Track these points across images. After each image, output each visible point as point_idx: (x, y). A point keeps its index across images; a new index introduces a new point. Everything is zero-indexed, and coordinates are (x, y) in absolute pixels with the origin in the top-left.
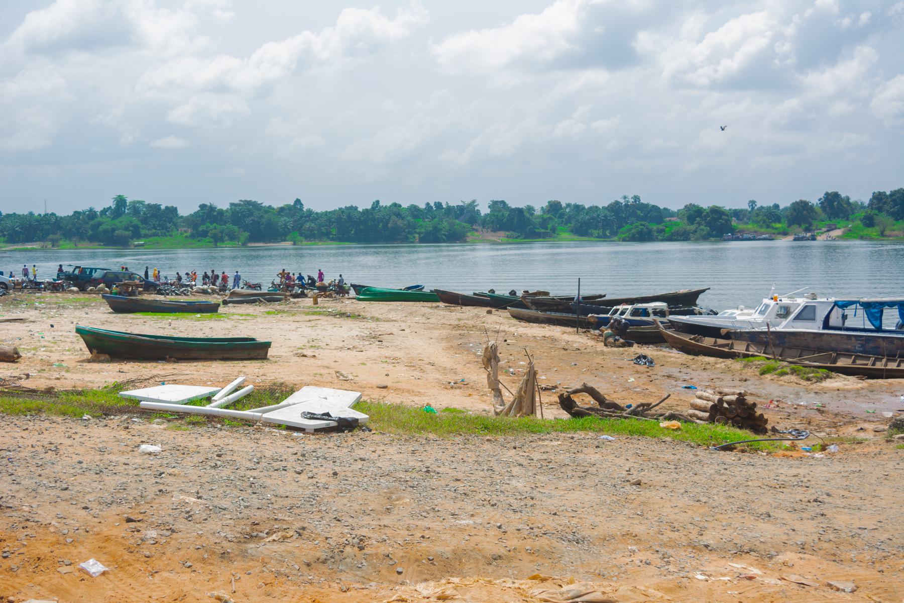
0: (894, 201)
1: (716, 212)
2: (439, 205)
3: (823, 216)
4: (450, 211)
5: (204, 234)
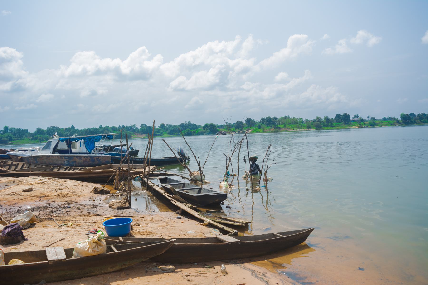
0: (267, 120)
1: (212, 125)
2: (123, 126)
3: (246, 126)
4: (127, 128)
5: (36, 139)
